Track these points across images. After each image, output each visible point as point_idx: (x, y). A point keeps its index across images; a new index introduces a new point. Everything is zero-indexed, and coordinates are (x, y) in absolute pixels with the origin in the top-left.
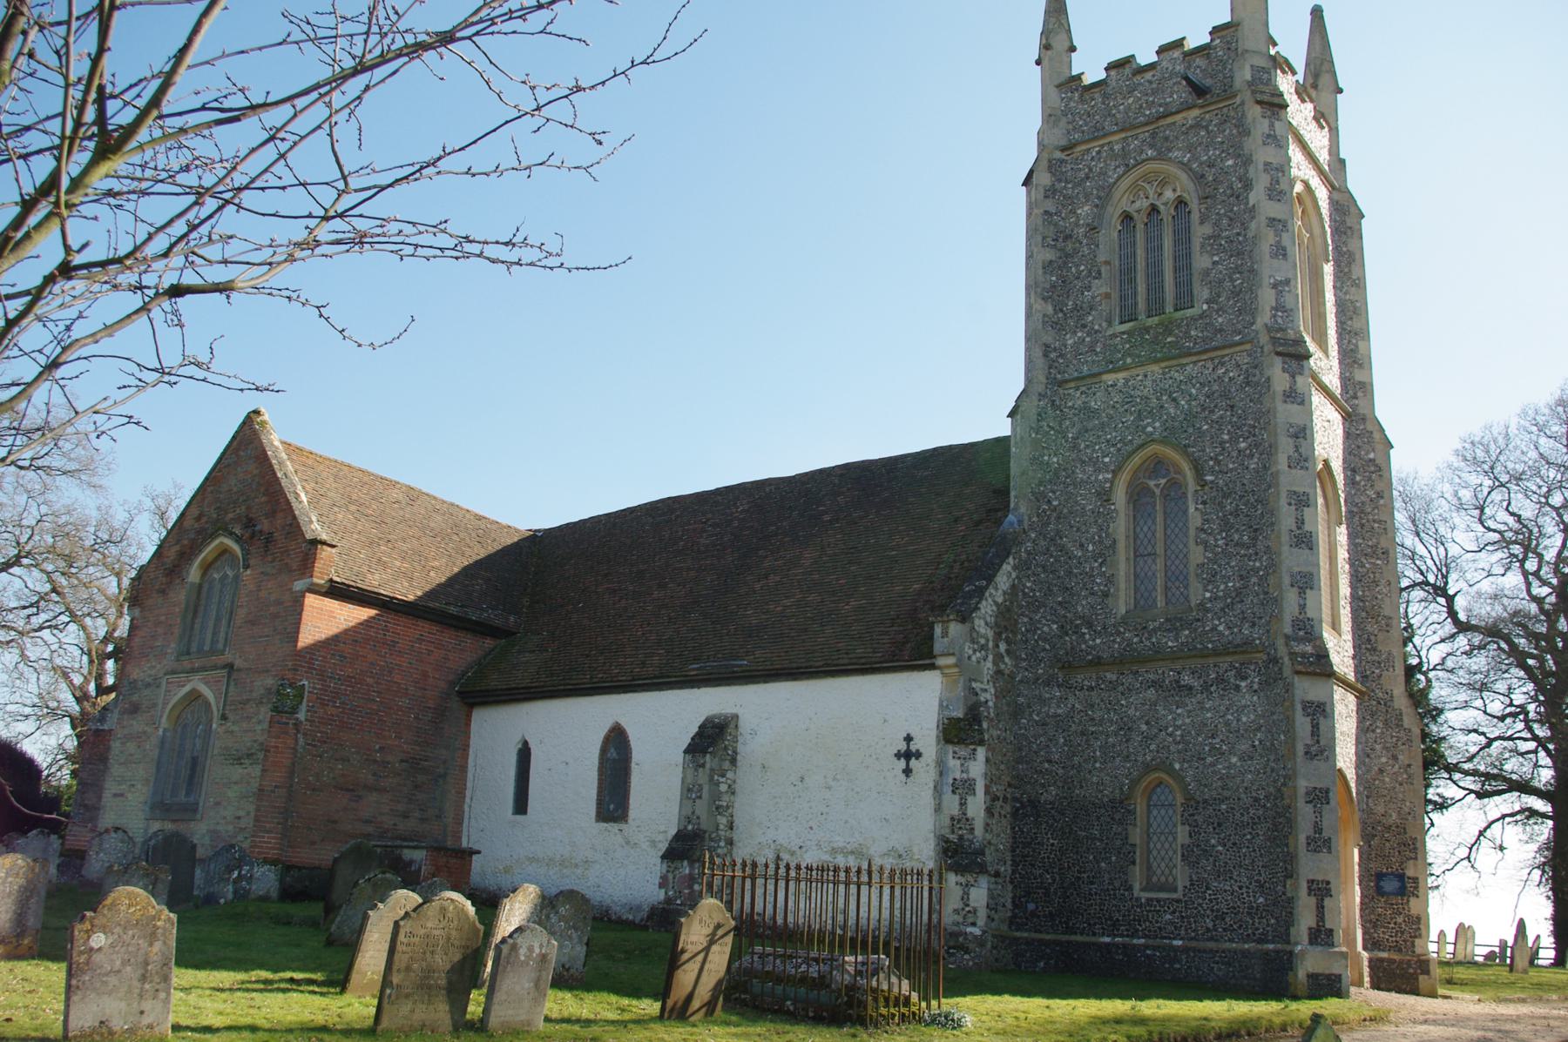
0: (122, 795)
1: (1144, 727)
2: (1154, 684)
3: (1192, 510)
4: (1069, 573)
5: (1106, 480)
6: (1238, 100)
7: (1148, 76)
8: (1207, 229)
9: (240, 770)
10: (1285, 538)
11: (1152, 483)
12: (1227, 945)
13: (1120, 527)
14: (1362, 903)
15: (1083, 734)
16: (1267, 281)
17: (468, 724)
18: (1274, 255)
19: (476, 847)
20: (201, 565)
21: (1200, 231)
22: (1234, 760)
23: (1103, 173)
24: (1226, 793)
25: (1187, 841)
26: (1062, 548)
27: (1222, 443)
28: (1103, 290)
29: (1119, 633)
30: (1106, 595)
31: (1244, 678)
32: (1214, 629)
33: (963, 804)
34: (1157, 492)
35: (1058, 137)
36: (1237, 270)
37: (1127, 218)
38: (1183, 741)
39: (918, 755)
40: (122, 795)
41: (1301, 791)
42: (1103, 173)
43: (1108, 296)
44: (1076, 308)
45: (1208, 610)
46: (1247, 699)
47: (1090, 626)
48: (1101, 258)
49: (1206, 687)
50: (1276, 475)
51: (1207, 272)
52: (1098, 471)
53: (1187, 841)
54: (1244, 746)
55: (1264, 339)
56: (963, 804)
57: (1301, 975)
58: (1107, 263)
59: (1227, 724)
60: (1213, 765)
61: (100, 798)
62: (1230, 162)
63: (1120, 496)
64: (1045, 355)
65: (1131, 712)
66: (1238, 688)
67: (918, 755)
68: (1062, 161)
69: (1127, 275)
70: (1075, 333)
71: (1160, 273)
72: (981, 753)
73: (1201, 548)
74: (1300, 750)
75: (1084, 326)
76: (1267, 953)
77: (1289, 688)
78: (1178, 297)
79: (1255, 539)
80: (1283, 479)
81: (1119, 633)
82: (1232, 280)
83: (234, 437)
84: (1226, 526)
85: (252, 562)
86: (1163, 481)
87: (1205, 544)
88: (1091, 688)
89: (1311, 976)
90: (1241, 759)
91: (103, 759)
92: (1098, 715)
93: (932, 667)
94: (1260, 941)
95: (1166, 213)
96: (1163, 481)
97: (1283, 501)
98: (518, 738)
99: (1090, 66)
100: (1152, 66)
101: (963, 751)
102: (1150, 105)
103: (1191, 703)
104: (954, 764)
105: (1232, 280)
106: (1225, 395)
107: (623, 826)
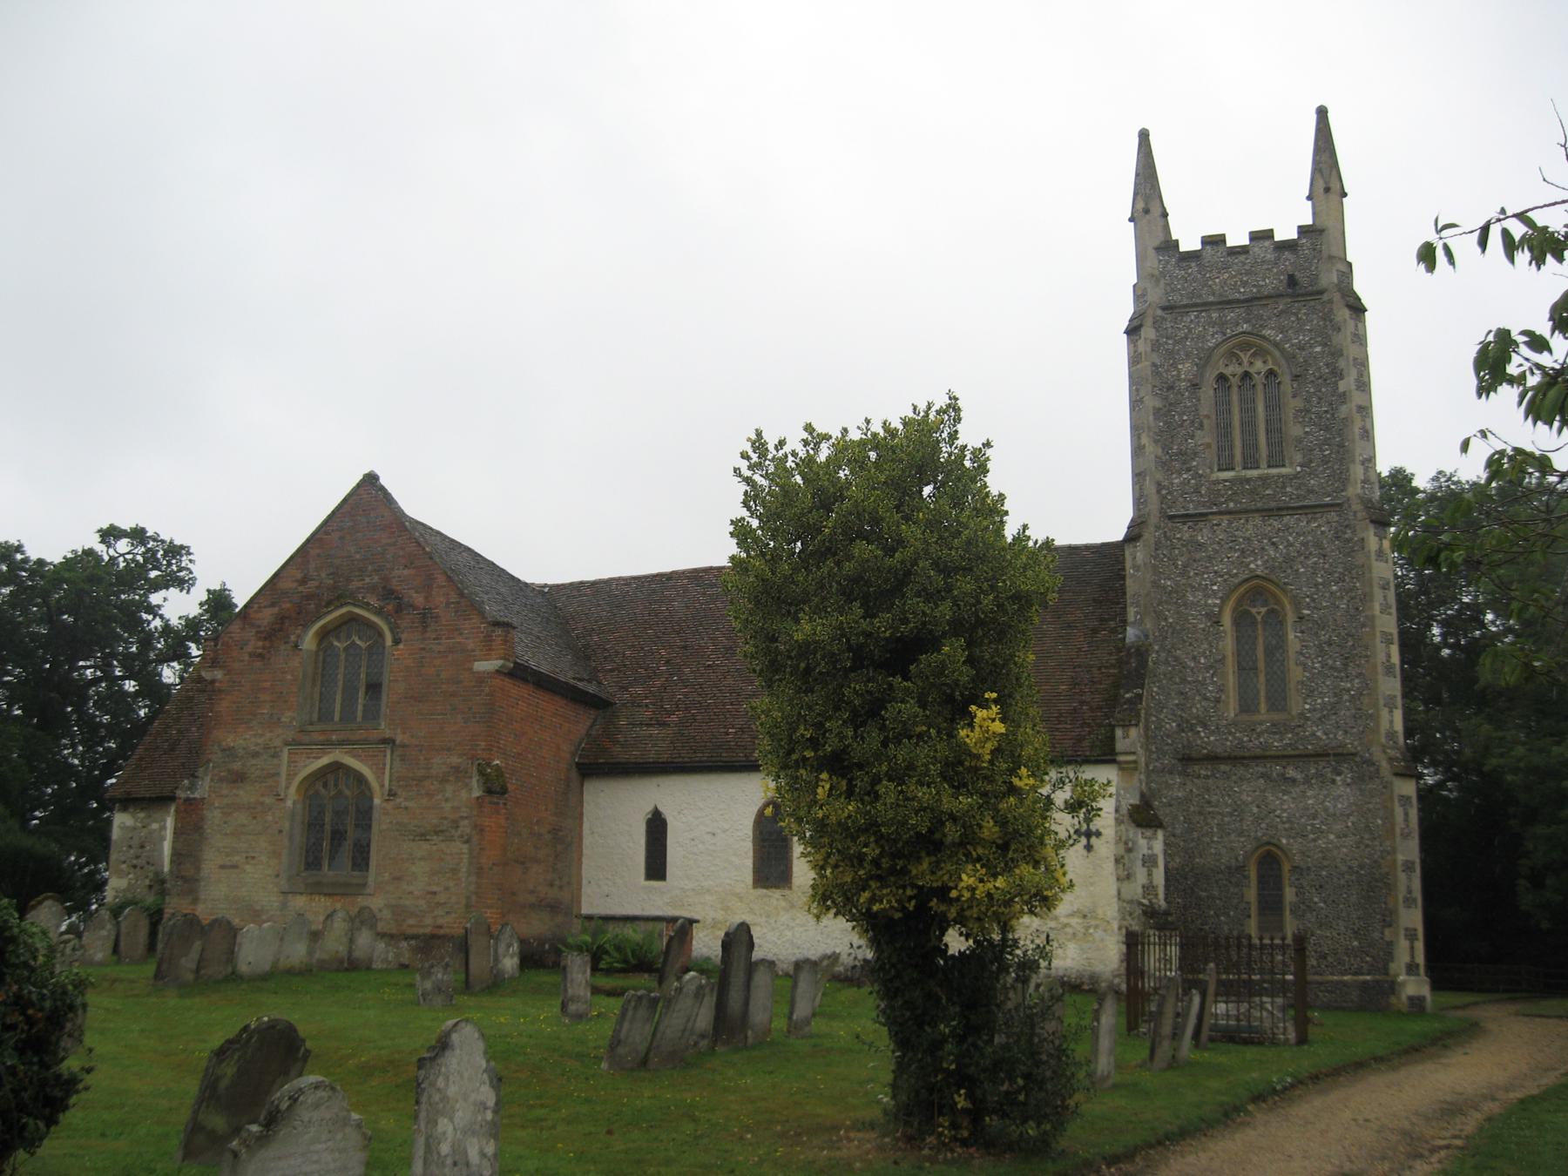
0: (235, 867)
1: (1255, 810)
2: (1263, 776)
3: (1291, 636)
4: (1184, 681)
5: (1215, 605)
6: (1325, 297)
7: (1242, 258)
8: (1298, 403)
9: (425, 846)
10: (1380, 669)
11: (1254, 611)
12: (1330, 978)
13: (1228, 644)
14: (173, 855)
15: (1200, 813)
16: (1359, 459)
17: (582, 793)
18: (1362, 438)
19: (696, 917)
20: (317, 633)
21: (1293, 404)
22: (1332, 837)
23: (1201, 337)
24: (1326, 863)
25: (1294, 899)
26: (1176, 659)
27: (1316, 585)
28: (1207, 440)
29: (1230, 733)
30: (1218, 701)
31: (1339, 774)
32: (1313, 734)
33: (1150, 875)
34: (1259, 618)
35: (1156, 295)
36: (1326, 442)
37: (1222, 378)
38: (1289, 821)
39: (1098, 834)
40: (235, 867)
41: (1400, 863)
42: (1201, 337)
43: (1209, 446)
44: (1181, 453)
45: (1308, 719)
46: (1341, 790)
47: (1205, 726)
48: (1204, 411)
49: (1307, 781)
50: (1372, 618)
51: (1299, 440)
52: (1207, 596)
53: (1294, 899)
54: (1338, 827)
55: (1356, 506)
56: (1150, 875)
57: (1404, 998)
58: (1208, 417)
59: (1326, 810)
60: (1314, 840)
61: (198, 869)
62: (1318, 349)
63: (1227, 620)
64: (1158, 492)
65: (1244, 797)
66: (1333, 782)
67: (1098, 834)
68: (1164, 319)
69: (1224, 431)
70: (1180, 474)
71: (1255, 435)
72: (1160, 834)
73: (1300, 668)
74: (1398, 831)
75: (1188, 470)
76: (1365, 982)
77: (1387, 786)
78: (1270, 456)
79: (1346, 665)
80: (1378, 622)
81: (1230, 733)
82: (1322, 450)
83: (345, 500)
84: (1321, 652)
85: (404, 636)
86: (1263, 610)
87: (1304, 665)
88: (1207, 777)
89: (1411, 998)
90: (1338, 837)
91: (198, 828)
92: (1214, 798)
93: (1113, 761)
94: (1356, 974)
95: (1259, 380)
96: (1263, 610)
97: (1378, 640)
98: (650, 808)
99: (1189, 242)
100: (1242, 250)
101: (1149, 833)
102: (1245, 284)
103: (1296, 791)
104: (1142, 842)
105: (1322, 450)
106: (1318, 545)
107: (787, 892)
